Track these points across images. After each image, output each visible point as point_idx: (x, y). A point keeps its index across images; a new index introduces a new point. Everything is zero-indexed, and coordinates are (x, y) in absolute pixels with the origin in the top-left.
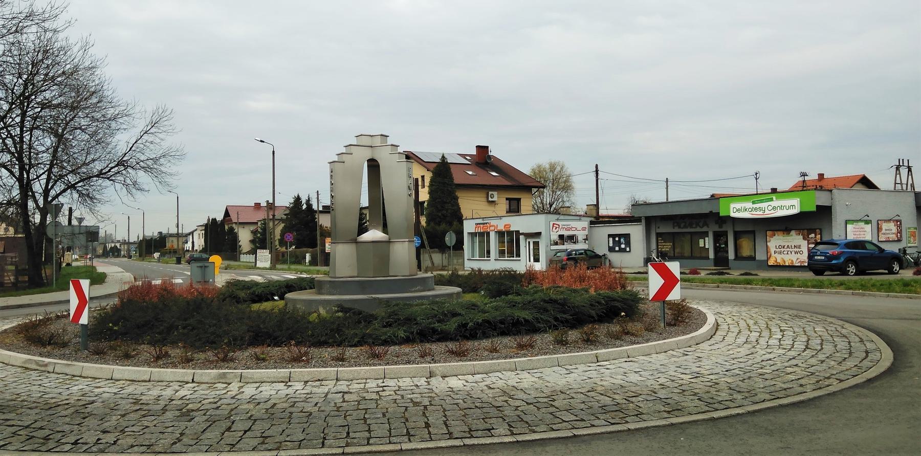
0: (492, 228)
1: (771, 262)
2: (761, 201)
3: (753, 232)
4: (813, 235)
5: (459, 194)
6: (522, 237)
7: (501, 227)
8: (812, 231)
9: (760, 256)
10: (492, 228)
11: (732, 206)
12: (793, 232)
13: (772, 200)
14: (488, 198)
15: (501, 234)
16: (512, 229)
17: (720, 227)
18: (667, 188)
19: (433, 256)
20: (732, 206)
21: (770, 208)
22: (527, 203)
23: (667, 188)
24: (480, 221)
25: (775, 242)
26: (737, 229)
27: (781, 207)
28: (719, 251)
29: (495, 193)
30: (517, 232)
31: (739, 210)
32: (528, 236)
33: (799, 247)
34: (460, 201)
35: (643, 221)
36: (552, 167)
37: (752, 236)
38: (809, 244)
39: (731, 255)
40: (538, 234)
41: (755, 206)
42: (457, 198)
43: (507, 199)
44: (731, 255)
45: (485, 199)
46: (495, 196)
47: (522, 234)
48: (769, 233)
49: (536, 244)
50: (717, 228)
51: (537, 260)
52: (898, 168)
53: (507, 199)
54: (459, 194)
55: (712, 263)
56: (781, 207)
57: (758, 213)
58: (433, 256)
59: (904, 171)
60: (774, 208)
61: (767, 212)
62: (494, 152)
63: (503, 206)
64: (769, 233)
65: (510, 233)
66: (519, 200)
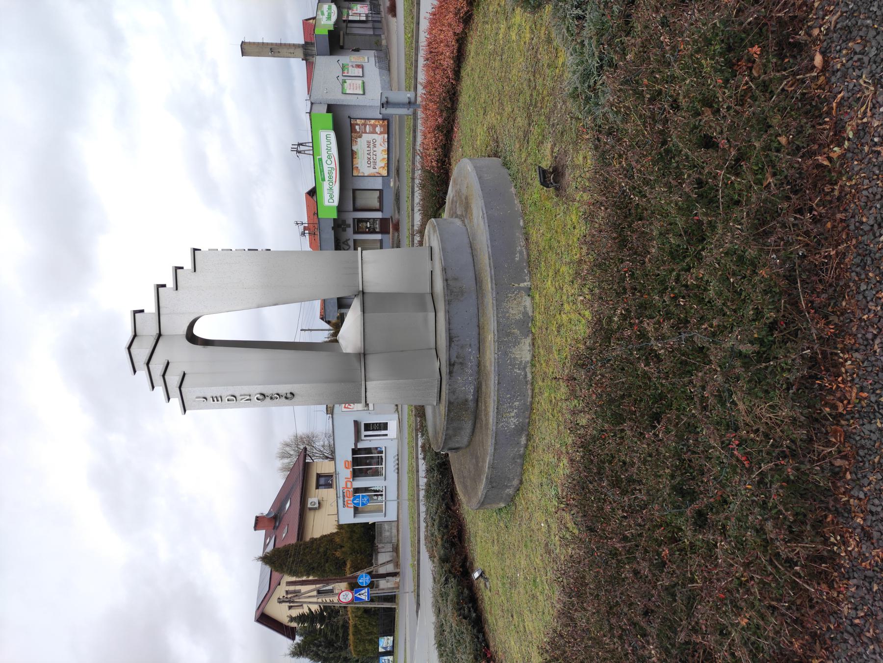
0: (349, 485)
1: (385, 173)
2: (322, 171)
3: (354, 191)
4: (357, 127)
5: (308, 538)
6: (360, 446)
7: (348, 473)
8: (352, 126)
9: (378, 184)
10: (349, 485)
11: (327, 203)
12: (354, 148)
13: (320, 160)
14: (315, 509)
15: (356, 474)
16: (350, 459)
17: (349, 226)
18: (311, 330)
19: (380, 562)
20: (327, 203)
21: (329, 162)
22: (323, 467)
23: (311, 330)
24: (341, 501)
25: (363, 166)
26: (351, 209)
27: (329, 149)
28: (374, 229)
29: (310, 500)
30: (355, 451)
31: (330, 198)
32: (358, 438)
33: (369, 142)
34: (315, 537)
35: (343, 311)
36: (284, 455)
37: (358, 192)
38: (366, 133)
39: (378, 215)
40: (357, 424)
41: (327, 179)
42: (313, 540)
43: (317, 488)
44: (378, 215)
45: (317, 512)
46: (312, 501)
47: (356, 445)
48: (355, 174)
49: (368, 427)
50: (350, 230)
51: (384, 426)
52: (300, 152)
53: (317, 488)
54: (308, 538)
55: (386, 236)
56: (329, 149)
57: (334, 175)
58: (380, 562)
59: (302, 148)
60: (329, 157)
61: (333, 165)
62: (265, 508)
63: (327, 494)
64: (355, 174)
65: (356, 462)
66: (319, 476)
